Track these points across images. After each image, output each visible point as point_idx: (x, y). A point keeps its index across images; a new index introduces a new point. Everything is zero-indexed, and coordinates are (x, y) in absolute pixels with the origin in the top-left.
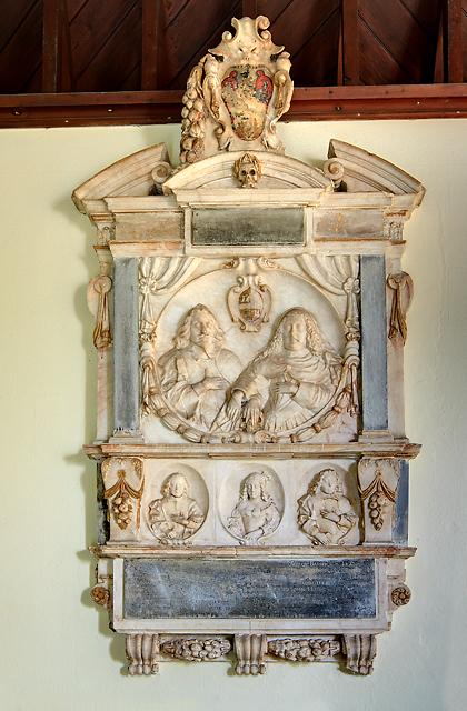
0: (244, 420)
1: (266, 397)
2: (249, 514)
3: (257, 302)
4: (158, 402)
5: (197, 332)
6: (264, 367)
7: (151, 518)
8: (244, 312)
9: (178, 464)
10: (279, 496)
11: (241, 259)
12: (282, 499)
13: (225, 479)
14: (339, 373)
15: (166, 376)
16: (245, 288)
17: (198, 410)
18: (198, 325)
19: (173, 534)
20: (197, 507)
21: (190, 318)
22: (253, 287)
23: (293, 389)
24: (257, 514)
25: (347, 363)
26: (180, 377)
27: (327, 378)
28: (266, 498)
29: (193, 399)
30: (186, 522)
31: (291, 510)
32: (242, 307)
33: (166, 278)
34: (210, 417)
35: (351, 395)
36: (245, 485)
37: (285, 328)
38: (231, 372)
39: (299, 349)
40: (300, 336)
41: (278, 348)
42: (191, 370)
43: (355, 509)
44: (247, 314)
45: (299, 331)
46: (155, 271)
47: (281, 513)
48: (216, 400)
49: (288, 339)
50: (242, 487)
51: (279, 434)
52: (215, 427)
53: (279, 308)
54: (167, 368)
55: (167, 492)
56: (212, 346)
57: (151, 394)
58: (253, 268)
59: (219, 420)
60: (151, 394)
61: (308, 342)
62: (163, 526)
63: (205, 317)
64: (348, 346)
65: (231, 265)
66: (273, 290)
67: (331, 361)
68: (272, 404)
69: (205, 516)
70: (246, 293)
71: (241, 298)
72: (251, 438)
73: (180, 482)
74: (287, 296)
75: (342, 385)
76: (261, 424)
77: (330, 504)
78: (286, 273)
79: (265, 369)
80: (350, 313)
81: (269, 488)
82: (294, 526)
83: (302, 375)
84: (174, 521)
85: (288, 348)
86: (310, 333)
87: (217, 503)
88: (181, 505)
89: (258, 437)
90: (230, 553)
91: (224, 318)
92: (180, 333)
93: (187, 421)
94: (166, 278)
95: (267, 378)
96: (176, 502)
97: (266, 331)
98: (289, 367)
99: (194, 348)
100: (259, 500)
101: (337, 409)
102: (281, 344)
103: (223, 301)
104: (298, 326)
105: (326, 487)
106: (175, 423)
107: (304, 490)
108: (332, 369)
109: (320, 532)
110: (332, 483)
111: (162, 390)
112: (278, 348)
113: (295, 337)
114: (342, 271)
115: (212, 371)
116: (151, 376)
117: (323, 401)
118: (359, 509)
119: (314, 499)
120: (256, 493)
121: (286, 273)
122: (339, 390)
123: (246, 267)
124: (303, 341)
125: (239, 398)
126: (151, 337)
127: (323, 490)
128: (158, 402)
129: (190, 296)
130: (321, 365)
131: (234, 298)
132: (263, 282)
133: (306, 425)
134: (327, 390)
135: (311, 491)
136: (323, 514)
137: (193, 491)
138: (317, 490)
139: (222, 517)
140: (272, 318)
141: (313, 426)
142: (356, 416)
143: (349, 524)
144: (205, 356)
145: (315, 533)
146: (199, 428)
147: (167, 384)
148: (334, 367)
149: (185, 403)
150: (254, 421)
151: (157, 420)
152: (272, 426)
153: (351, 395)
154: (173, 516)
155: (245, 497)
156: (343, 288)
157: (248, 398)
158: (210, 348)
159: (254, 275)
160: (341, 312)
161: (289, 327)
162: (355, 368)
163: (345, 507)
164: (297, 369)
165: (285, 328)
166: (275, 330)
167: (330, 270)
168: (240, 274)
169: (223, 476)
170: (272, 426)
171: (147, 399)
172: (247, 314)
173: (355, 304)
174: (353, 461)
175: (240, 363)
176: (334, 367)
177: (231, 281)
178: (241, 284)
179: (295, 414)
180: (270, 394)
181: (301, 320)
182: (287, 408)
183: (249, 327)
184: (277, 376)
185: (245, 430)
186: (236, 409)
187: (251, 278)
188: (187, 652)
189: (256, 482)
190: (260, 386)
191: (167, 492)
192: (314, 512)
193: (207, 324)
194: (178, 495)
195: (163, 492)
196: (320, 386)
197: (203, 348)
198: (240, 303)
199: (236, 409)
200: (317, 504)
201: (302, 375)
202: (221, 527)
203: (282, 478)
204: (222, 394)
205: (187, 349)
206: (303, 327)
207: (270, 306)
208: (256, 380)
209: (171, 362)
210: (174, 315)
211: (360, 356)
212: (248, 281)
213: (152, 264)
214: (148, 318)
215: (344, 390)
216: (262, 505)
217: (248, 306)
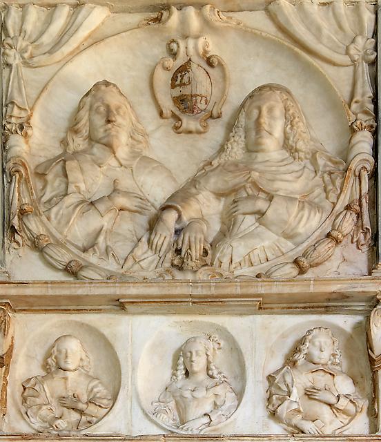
0: (178, 252)
1: (216, 227)
2: (187, 394)
3: (201, 82)
4: (34, 225)
5: (99, 121)
6: (213, 180)
7: (24, 400)
8: (181, 101)
9: (70, 322)
10: (237, 370)
11: (174, 9)
12: (242, 376)
13: (147, 345)
14: (338, 182)
15: (49, 189)
16: (181, 61)
17: (101, 239)
18: (102, 109)
19: (62, 424)
20: (100, 388)
21: (89, 99)
22: (195, 59)
23: (261, 205)
24: (200, 394)
25: (353, 166)
26: (72, 188)
27: (318, 191)
28: (215, 373)
29: (94, 221)
30: (81, 406)
31: (255, 389)
32: (177, 92)
33: (47, 39)
34: (122, 249)
35: (359, 215)
36: (182, 361)
37: (248, 116)
38: (157, 189)
39: (271, 145)
40: (276, 128)
41: (237, 151)
42: (90, 179)
43: (362, 390)
44: (185, 103)
45: (272, 117)
46: (29, 27)
47: (240, 395)
48: (130, 226)
49: (253, 133)
50: (176, 358)
51: (237, 273)
52: (130, 262)
53: (236, 96)
54: (50, 177)
55: (53, 365)
56: (126, 149)
57: (23, 213)
58: (195, 23)
59: (138, 252)
60: (23, 213)
61: (286, 138)
62: (44, 411)
63: (113, 99)
64: (353, 141)
65: (158, 20)
66: (229, 68)
67: (325, 166)
68: (228, 229)
69: (115, 399)
70: (184, 69)
71: (174, 78)
72: (190, 277)
73: (74, 349)
74: (249, 70)
75: (344, 200)
76: (208, 259)
77: (322, 380)
78: (250, 34)
79: (215, 182)
80: (359, 90)
81: (221, 361)
82: (261, 412)
83: (278, 185)
84: (63, 405)
85: (253, 148)
86: (290, 121)
87: (133, 378)
88: (76, 383)
89: (203, 275)
90: (220, 105)
91: (148, 112)
92: (73, 129)
93: (83, 255)
94: (47, 39)
95: (219, 195)
96: (66, 378)
97: (216, 131)
98: (255, 175)
99: (95, 150)
100: (202, 376)
101: (335, 233)
102: (242, 145)
103: (145, 85)
104: (270, 110)
105: (316, 353)
106: (63, 257)
107: (277, 362)
108: (327, 177)
109: (303, 419)
110: (324, 348)
111: (42, 209)
112: (237, 151)
113: (266, 127)
114: (347, 25)
115: (126, 183)
116: (23, 187)
117: (310, 224)
118: (368, 389)
119: (294, 372)
120: (199, 364)
121: (250, 34)
122: (340, 206)
123: (184, 22)
124: (278, 132)
125: (171, 218)
126: (22, 128)
127: (310, 359)
128: (34, 225)
129: (85, 70)
130: (309, 173)
131: (163, 78)
132: (213, 50)
133: (282, 260)
134: (317, 207)
135: (290, 362)
136: (309, 394)
137: (94, 362)
138: (300, 358)
139: (142, 398)
140: (227, 111)
141: (296, 262)
142: (365, 249)
143: (351, 408)
144: (113, 162)
145: (297, 420)
146: (103, 265)
147: (49, 201)
148: (330, 173)
149: (79, 228)
150: (196, 252)
151: (34, 256)
152: (226, 261)
153: (359, 215)
154: (62, 400)
155: (181, 373)
156: (347, 53)
157: (185, 218)
158: (122, 152)
159: (197, 37)
160: (344, 91)
161: (255, 112)
162: (365, 176)
163: (345, 386)
164: (269, 176)
165: (248, 116)
166: (231, 127)
167: (327, 28)
168: (174, 35)
169: (147, 340)
170: (226, 261)
171: (15, 222)
172: (185, 103)
173: (367, 78)
174: (360, 318)
175: (171, 176)
176: (330, 173)
177: (159, 51)
178: (174, 55)
179: (267, 243)
180: (223, 223)
181: (276, 103)
182: (251, 235)
183: (189, 123)
184: (235, 190)
185: (180, 268)
186: (165, 237)
187: (191, 43)
188: (92, 409)
189: (200, 347)
190: (206, 208)
191: (53, 365)
192: (295, 391)
193: (118, 108)
194: (71, 367)
195: (46, 366)
196: (307, 202)
197: (109, 146)
198: (173, 86)
199: (165, 237)
200: (301, 380)
201: (278, 185)
202: (140, 414)
203: (243, 342)
204: (143, 220)
205: (84, 152)
206: (278, 112)
207: (223, 92)
208: (200, 197)
209: (58, 168)
210: (61, 103)
211: (376, 156)
212: (187, 49)
213: (23, 19)
214: (18, 100)
215: (348, 208)
216: (210, 382)
217: (186, 91)
